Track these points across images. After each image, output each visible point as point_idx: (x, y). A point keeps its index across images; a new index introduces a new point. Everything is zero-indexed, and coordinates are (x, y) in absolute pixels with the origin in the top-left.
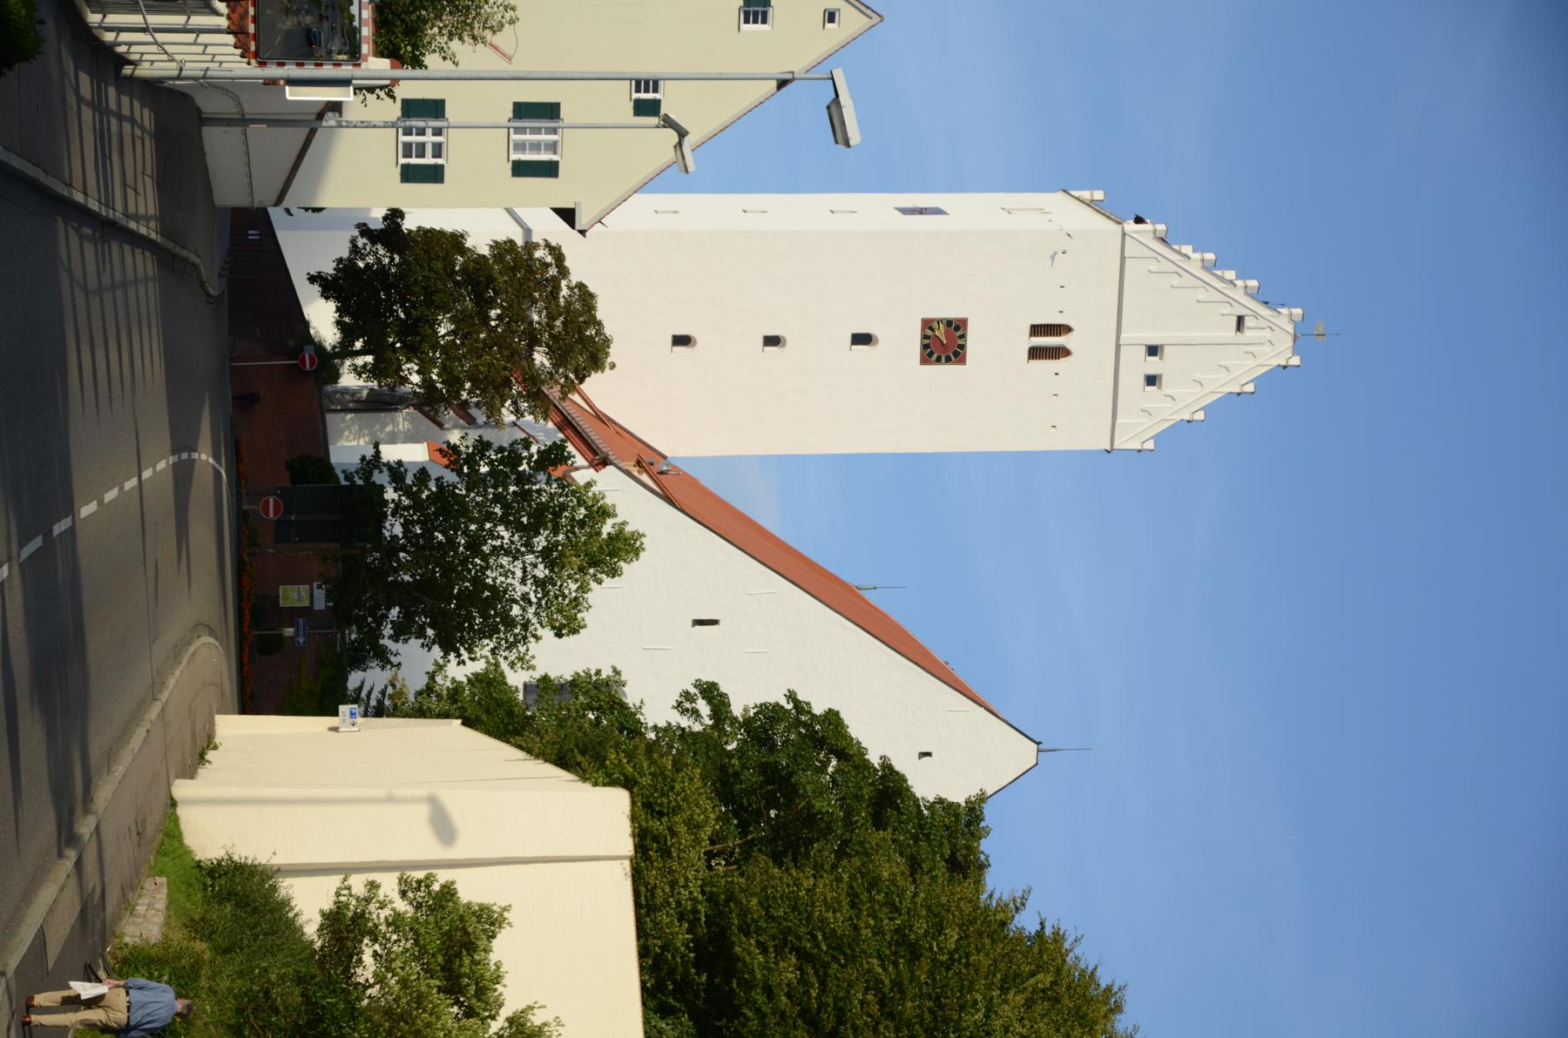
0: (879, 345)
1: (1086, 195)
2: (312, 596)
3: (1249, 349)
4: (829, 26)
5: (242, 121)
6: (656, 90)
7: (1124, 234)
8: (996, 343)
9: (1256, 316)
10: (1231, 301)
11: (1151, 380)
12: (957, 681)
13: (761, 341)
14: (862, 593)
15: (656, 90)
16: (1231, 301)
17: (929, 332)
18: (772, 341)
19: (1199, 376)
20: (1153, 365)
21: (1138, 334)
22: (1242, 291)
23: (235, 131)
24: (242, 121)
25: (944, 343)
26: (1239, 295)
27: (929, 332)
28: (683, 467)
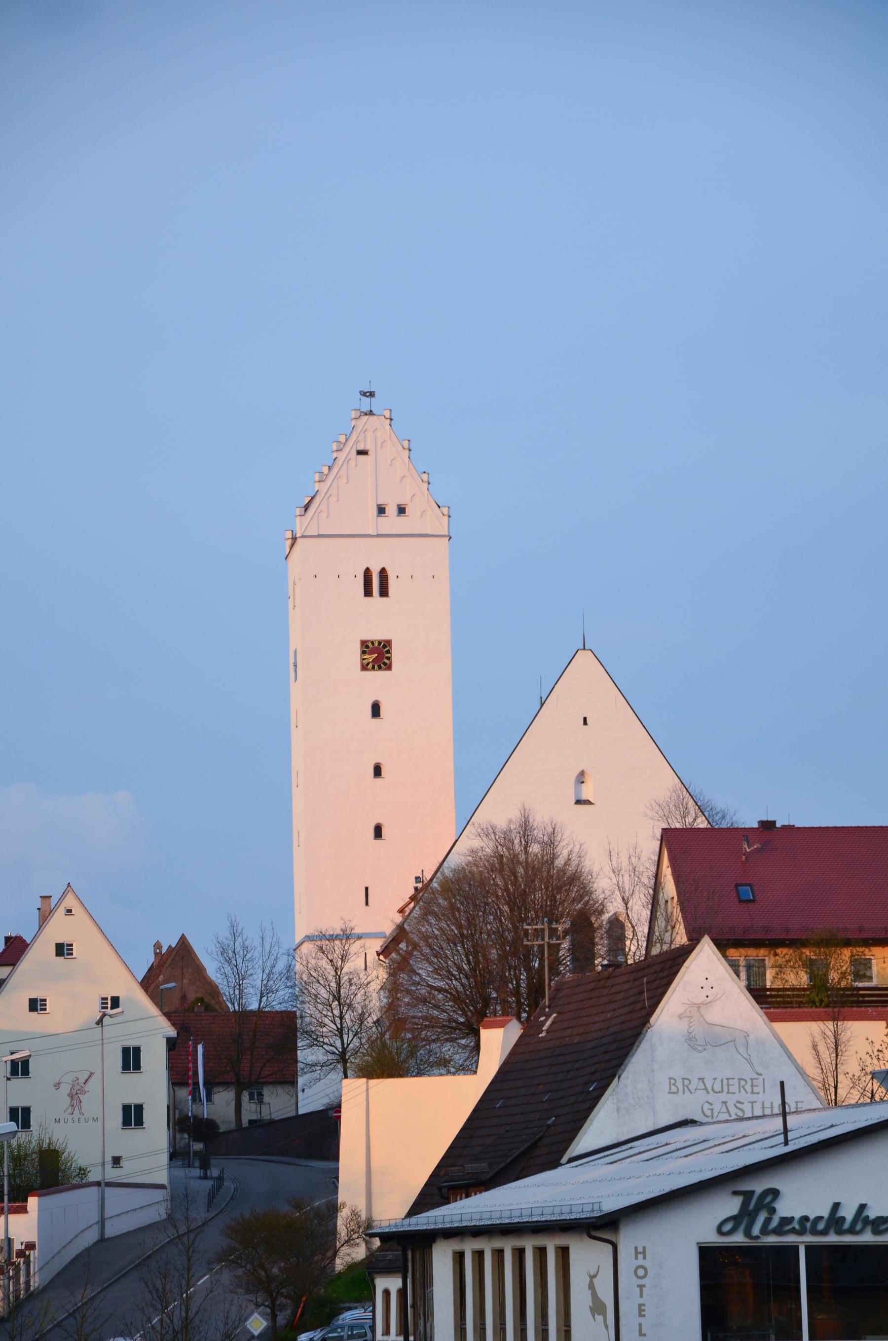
0: (379, 699)
3: (379, 445)
4: (73, 912)
5: (102, 1222)
6: (107, 999)
7: (303, 537)
8: (377, 619)
9: (357, 442)
10: (347, 460)
11: (402, 510)
16: (347, 460)
17: (370, 666)
18: (378, 771)
20: (391, 510)
21: (370, 522)
22: (340, 453)
24: (102, 1222)
25: (377, 655)
26: (342, 456)
27: (370, 666)
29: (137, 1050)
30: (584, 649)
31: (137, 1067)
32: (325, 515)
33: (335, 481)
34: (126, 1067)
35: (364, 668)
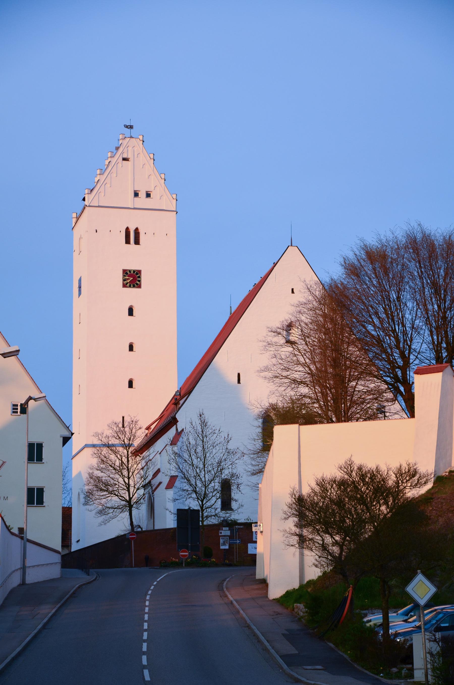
0: (133, 305)
1: (74, 220)
2: (224, 536)
3: (136, 156)
5: (24, 568)
6: (17, 405)
7: (89, 206)
8: (133, 258)
9: (122, 153)
10: (117, 163)
11: (148, 195)
12: (265, 277)
13: (131, 352)
14: (232, 312)
15: (17, 405)
16: (117, 163)
17: (128, 285)
19: (147, 177)
20: (142, 194)
21: (130, 201)
22: (112, 158)
23: (28, 571)
24: (24, 568)
25: (132, 279)
26: (114, 160)
27: (128, 285)
28: (181, 385)
29: (40, 446)
30: (292, 246)
31: (40, 459)
32: (103, 194)
33: (115, 165)
34: (30, 459)
35: (124, 286)
